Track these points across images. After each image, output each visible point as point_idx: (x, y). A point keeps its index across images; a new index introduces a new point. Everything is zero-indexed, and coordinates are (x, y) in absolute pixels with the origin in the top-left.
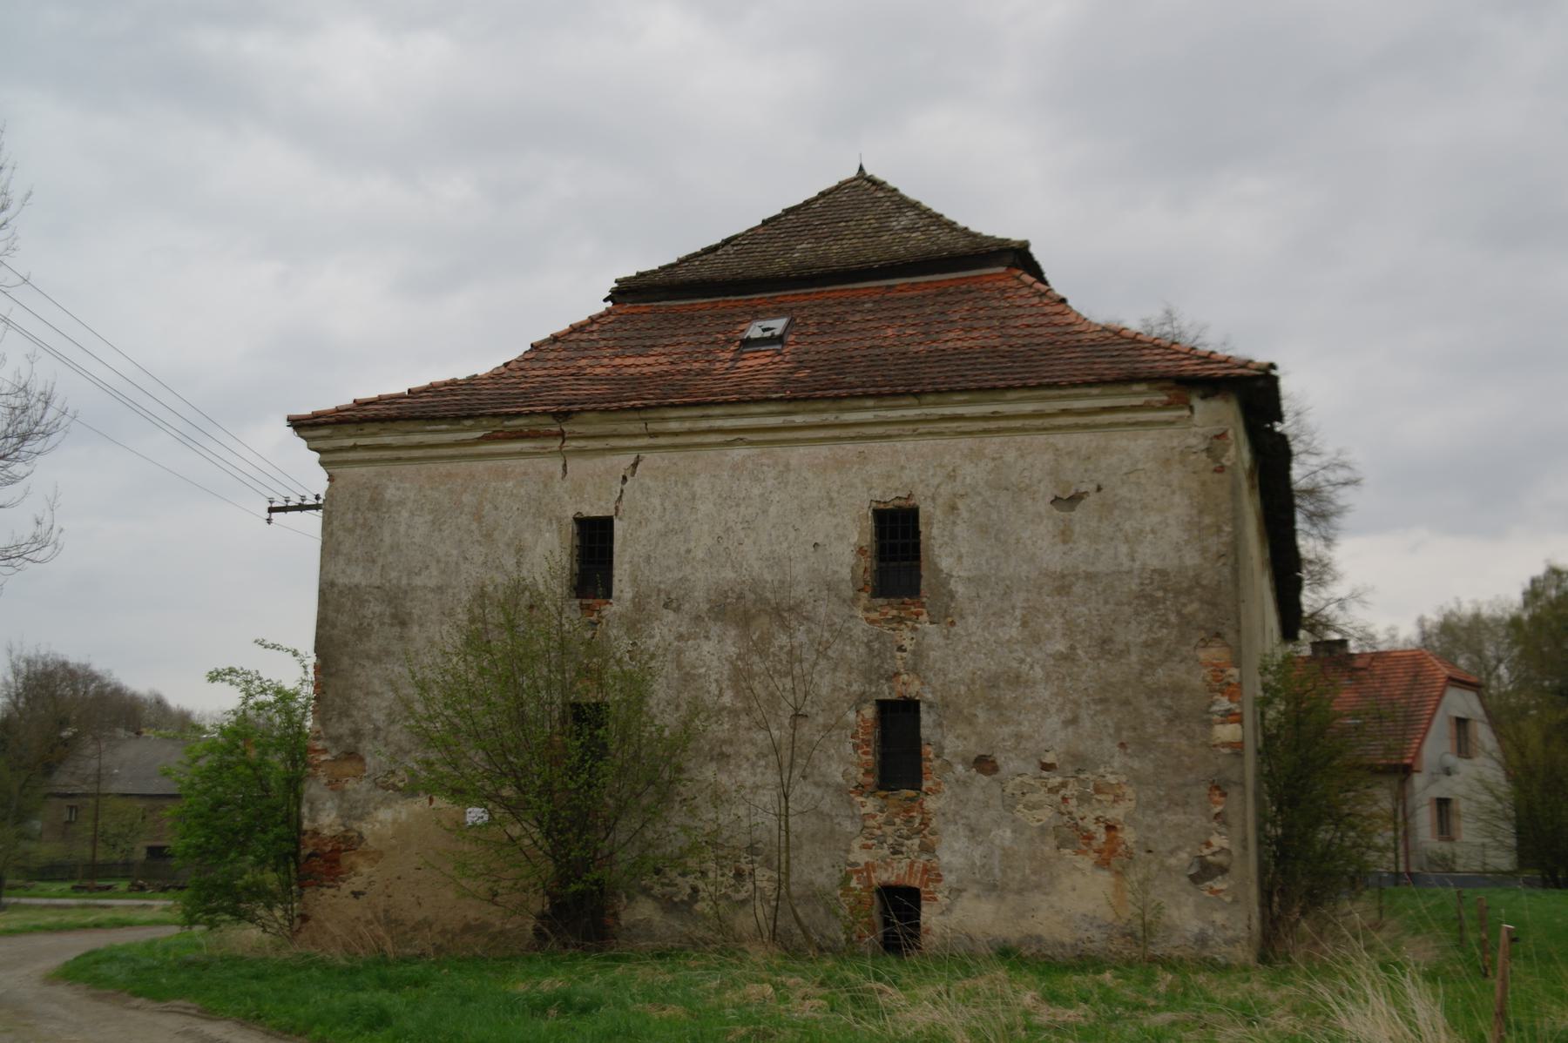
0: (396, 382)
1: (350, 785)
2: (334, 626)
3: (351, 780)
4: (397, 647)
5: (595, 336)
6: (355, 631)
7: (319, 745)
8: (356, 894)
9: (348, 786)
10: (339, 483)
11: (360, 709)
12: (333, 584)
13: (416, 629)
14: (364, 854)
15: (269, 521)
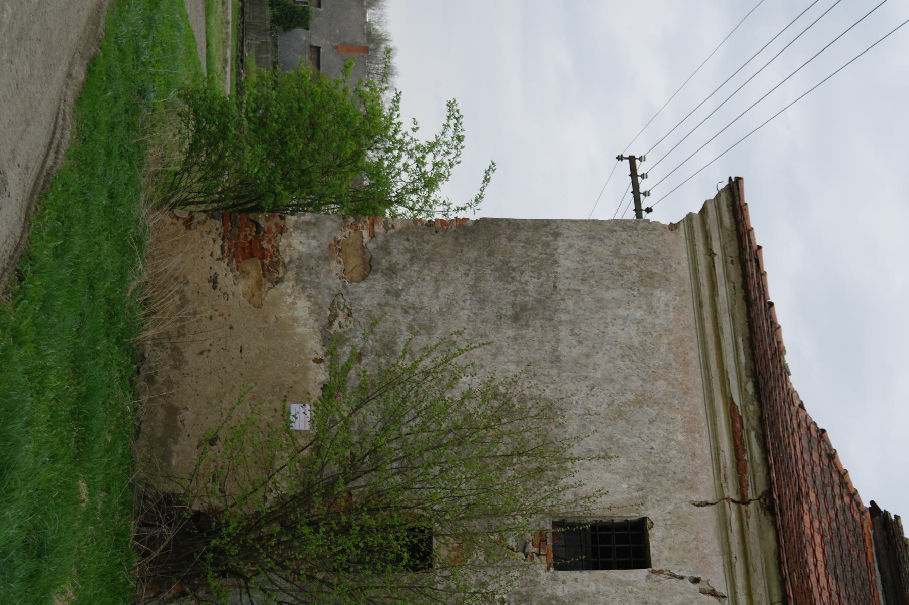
0: (780, 290)
1: (336, 267)
2: (510, 239)
3: (341, 266)
4: (490, 311)
5: (838, 502)
6: (505, 263)
7: (379, 229)
8: (214, 281)
9: (334, 263)
10: (669, 237)
11: (419, 272)
12: (556, 235)
13: (511, 333)
14: (259, 285)
15: (620, 158)
